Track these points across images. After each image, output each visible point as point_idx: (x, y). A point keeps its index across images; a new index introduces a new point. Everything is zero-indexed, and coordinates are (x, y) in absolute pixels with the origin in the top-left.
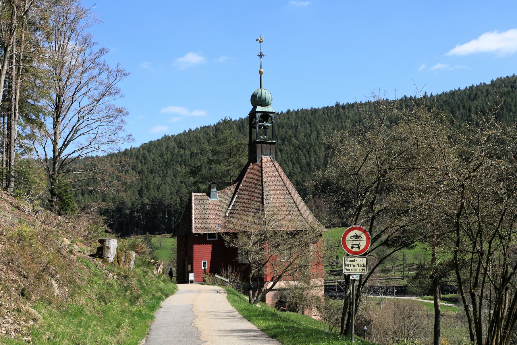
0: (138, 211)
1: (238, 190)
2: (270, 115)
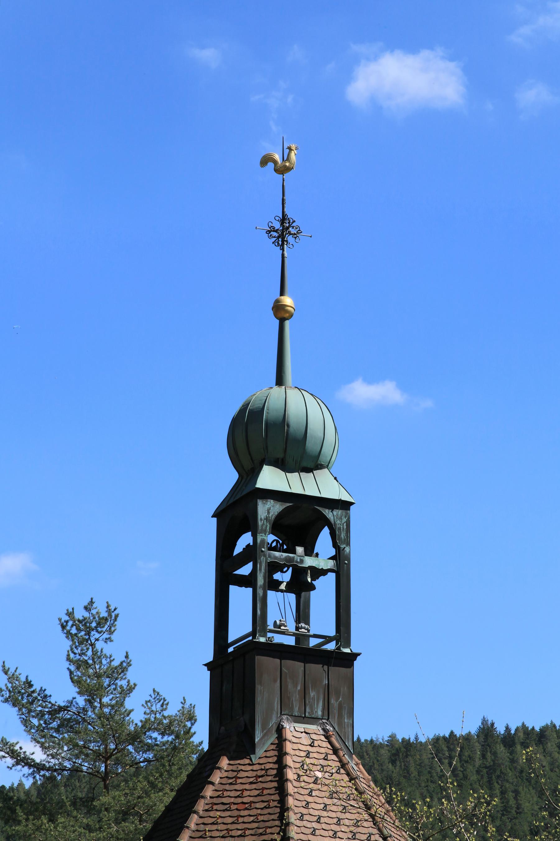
2: (329, 514)
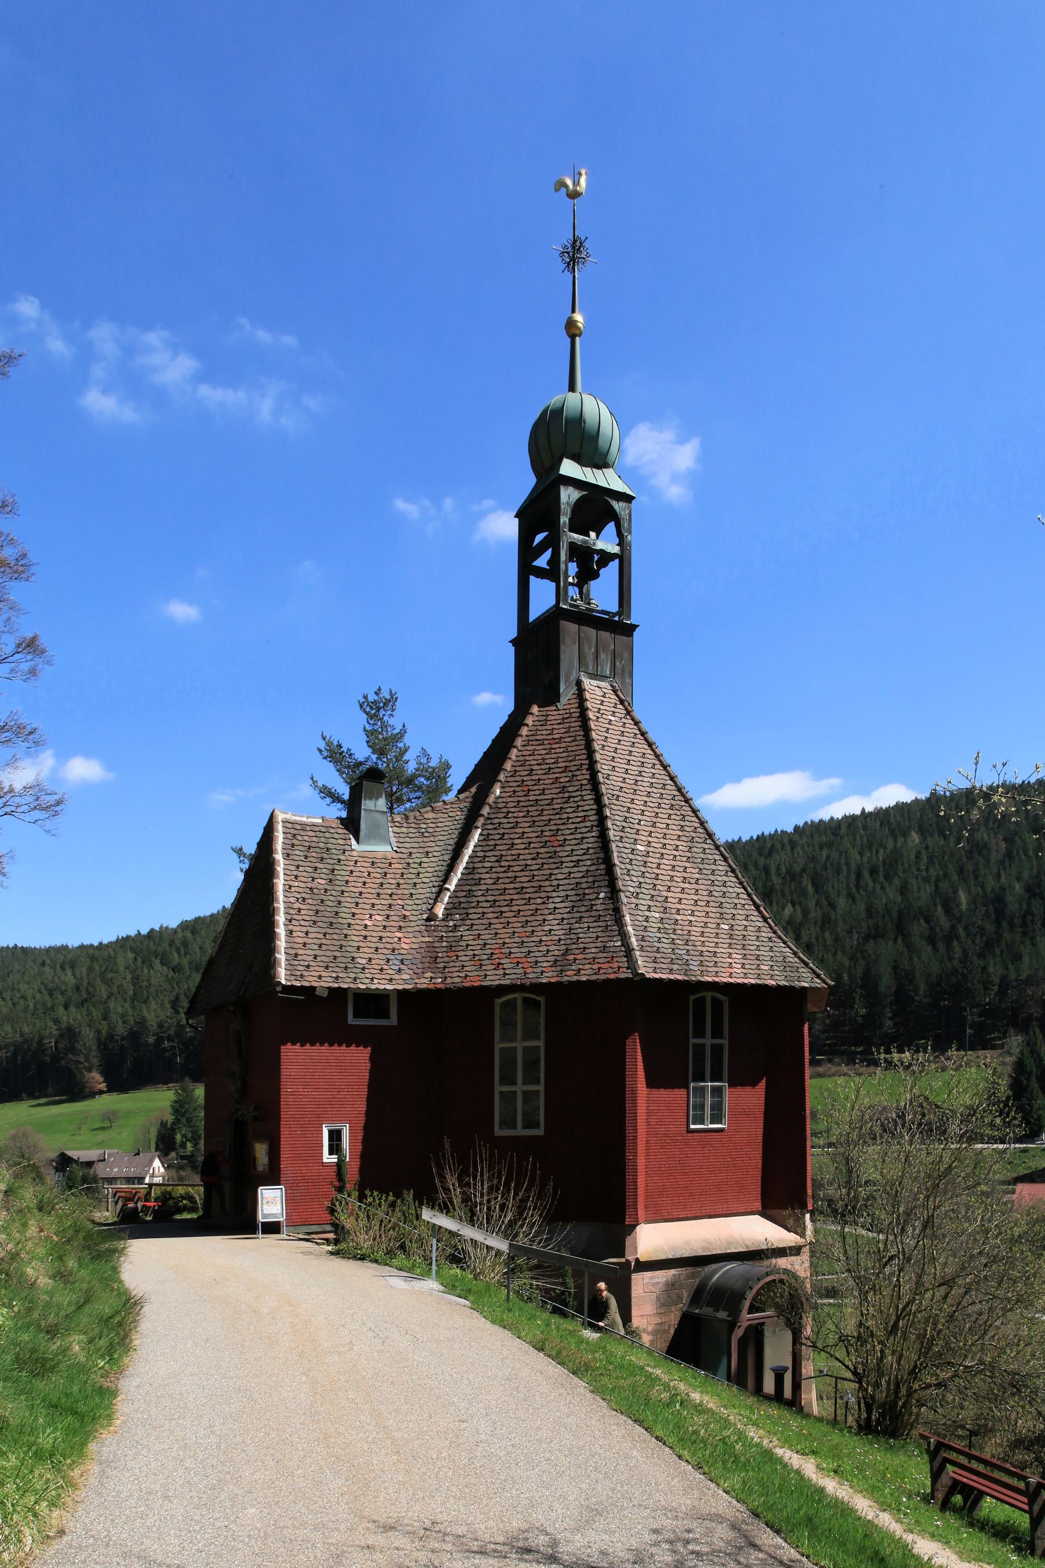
0: (170, 1039)
1: (485, 810)
2: (618, 506)
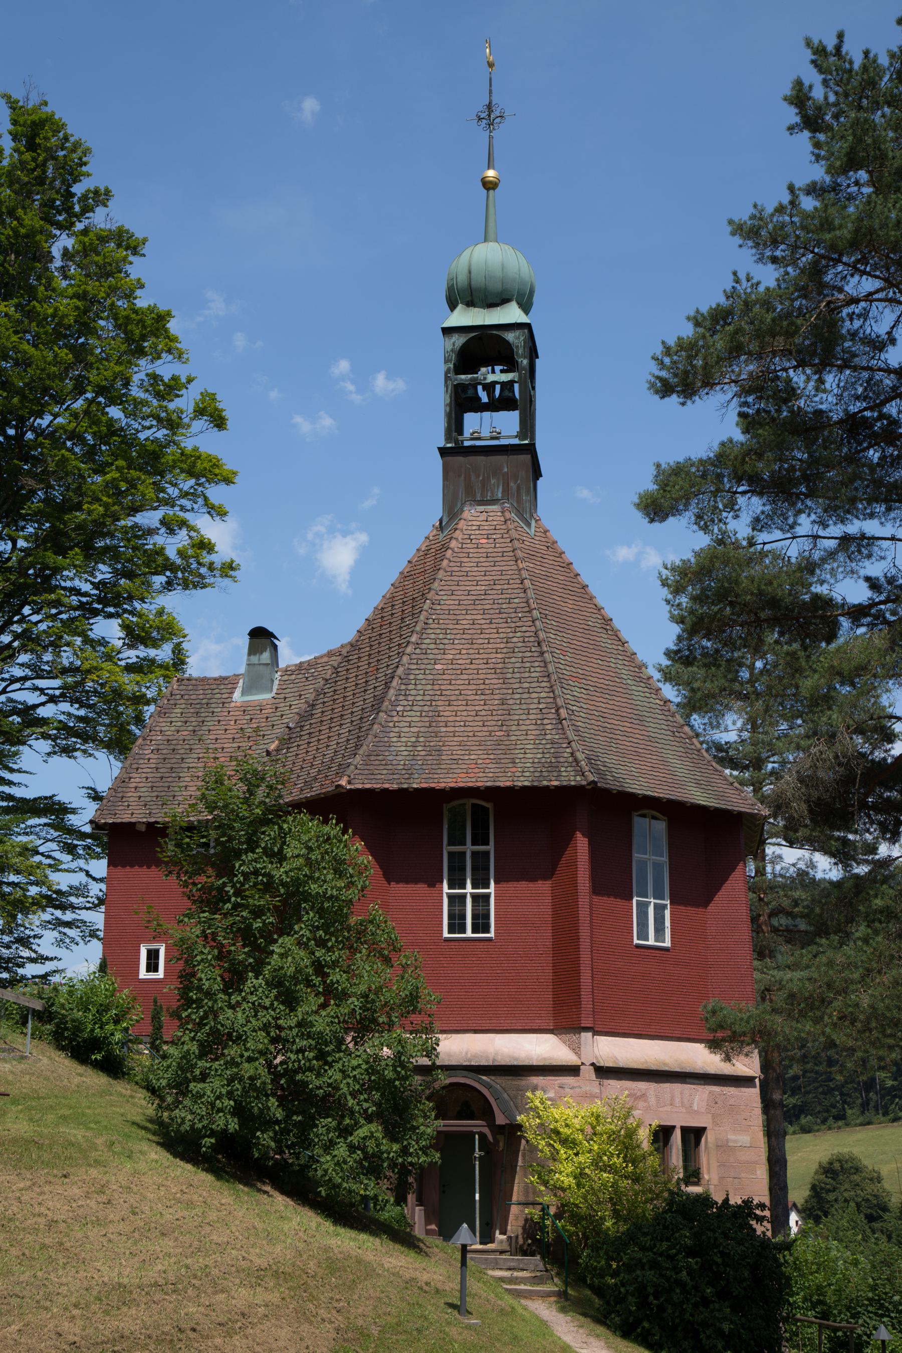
2: (510, 336)
